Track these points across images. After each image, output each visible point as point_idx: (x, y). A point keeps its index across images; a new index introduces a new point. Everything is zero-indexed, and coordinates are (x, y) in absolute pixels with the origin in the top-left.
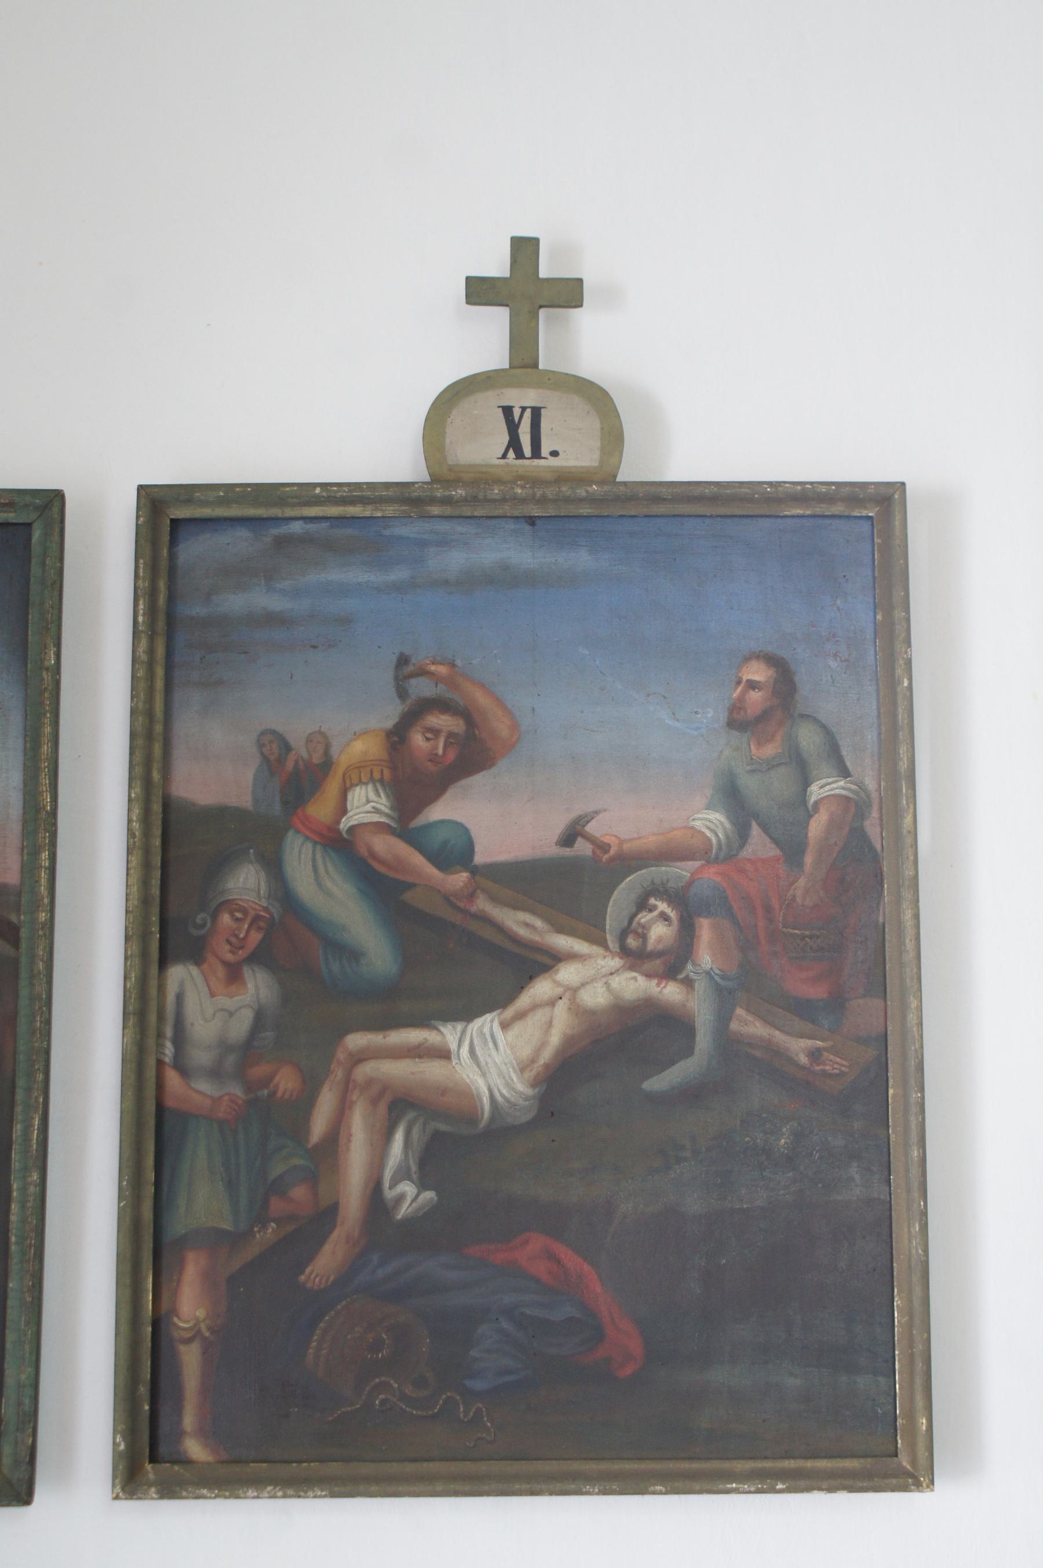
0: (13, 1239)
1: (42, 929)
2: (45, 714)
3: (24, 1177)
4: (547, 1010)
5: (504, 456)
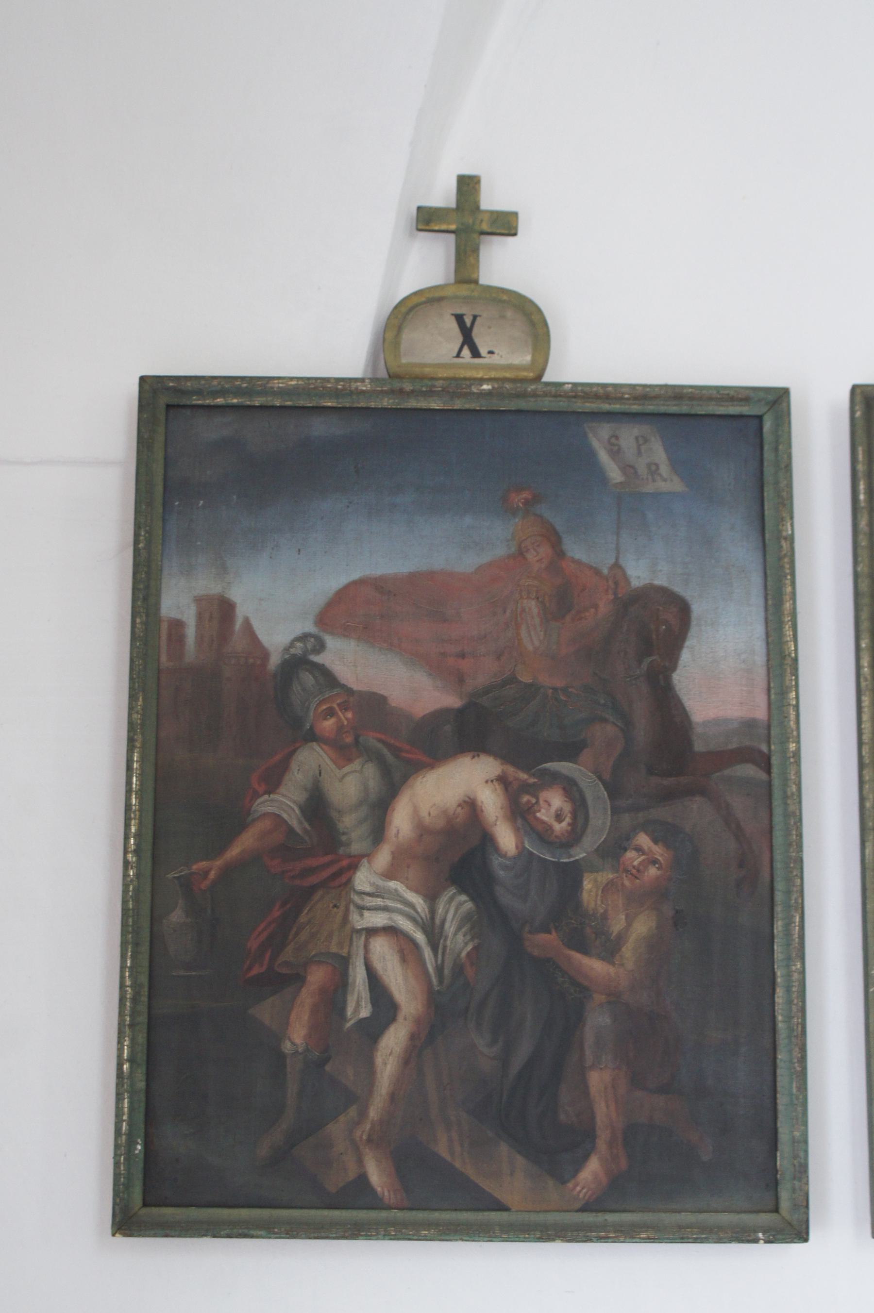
0: (780, 1018)
1: (793, 757)
2: (786, 577)
3: (788, 966)
5: (458, 355)
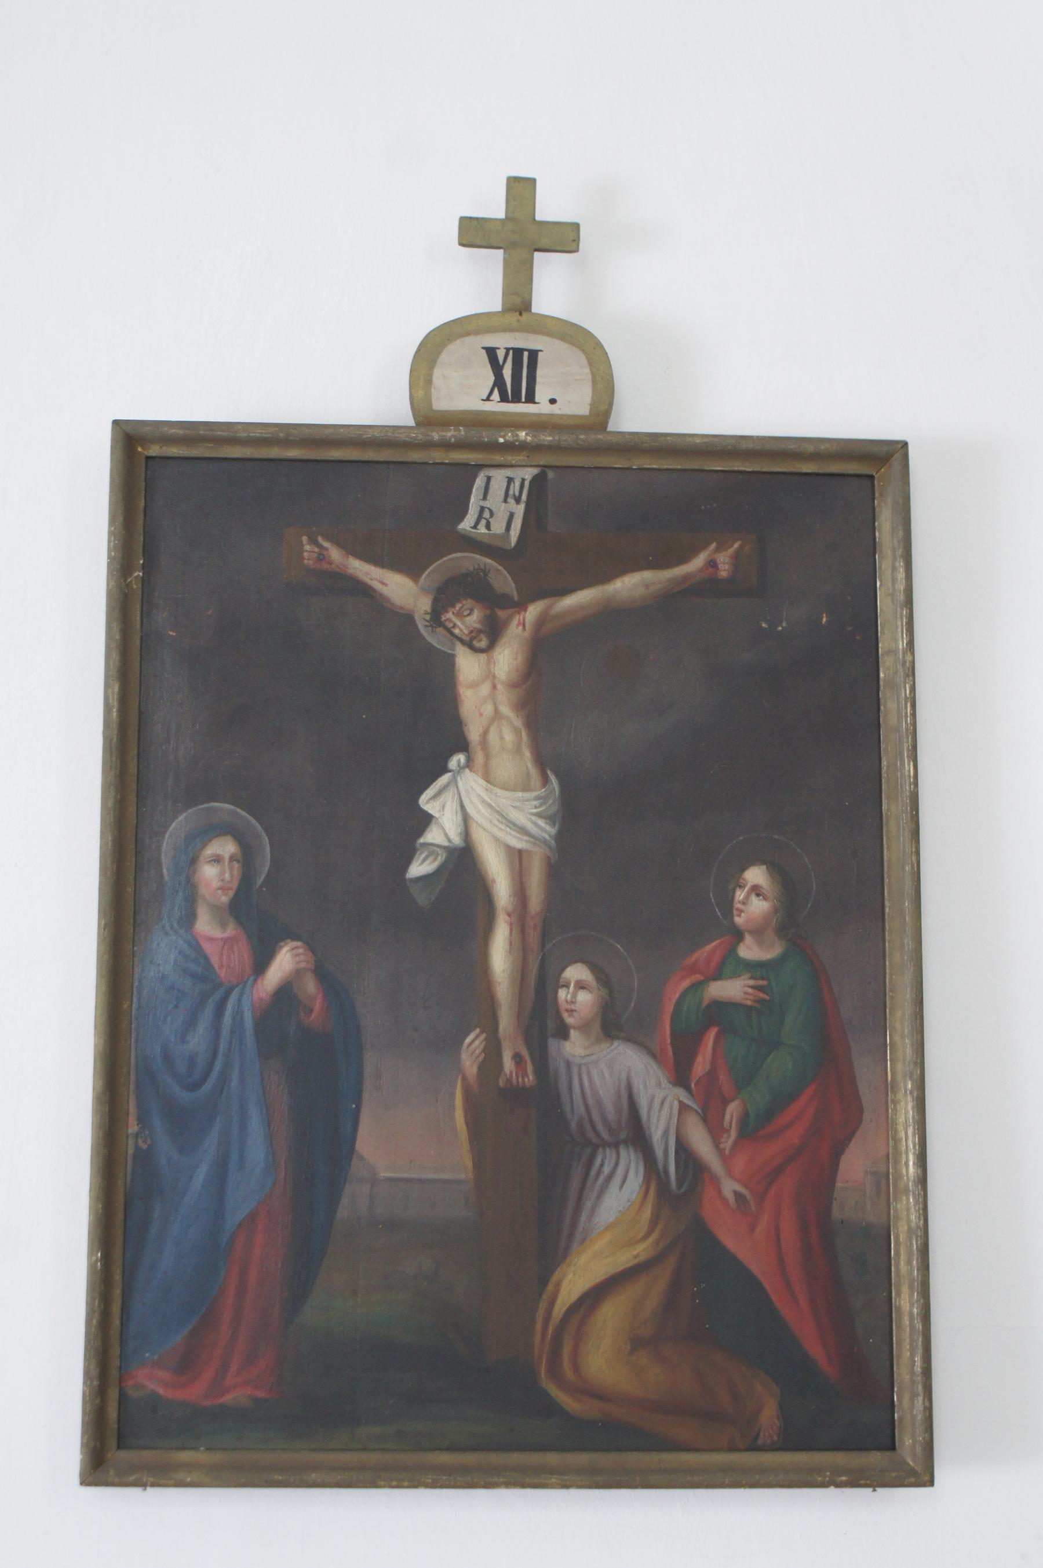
4: (452, 790)
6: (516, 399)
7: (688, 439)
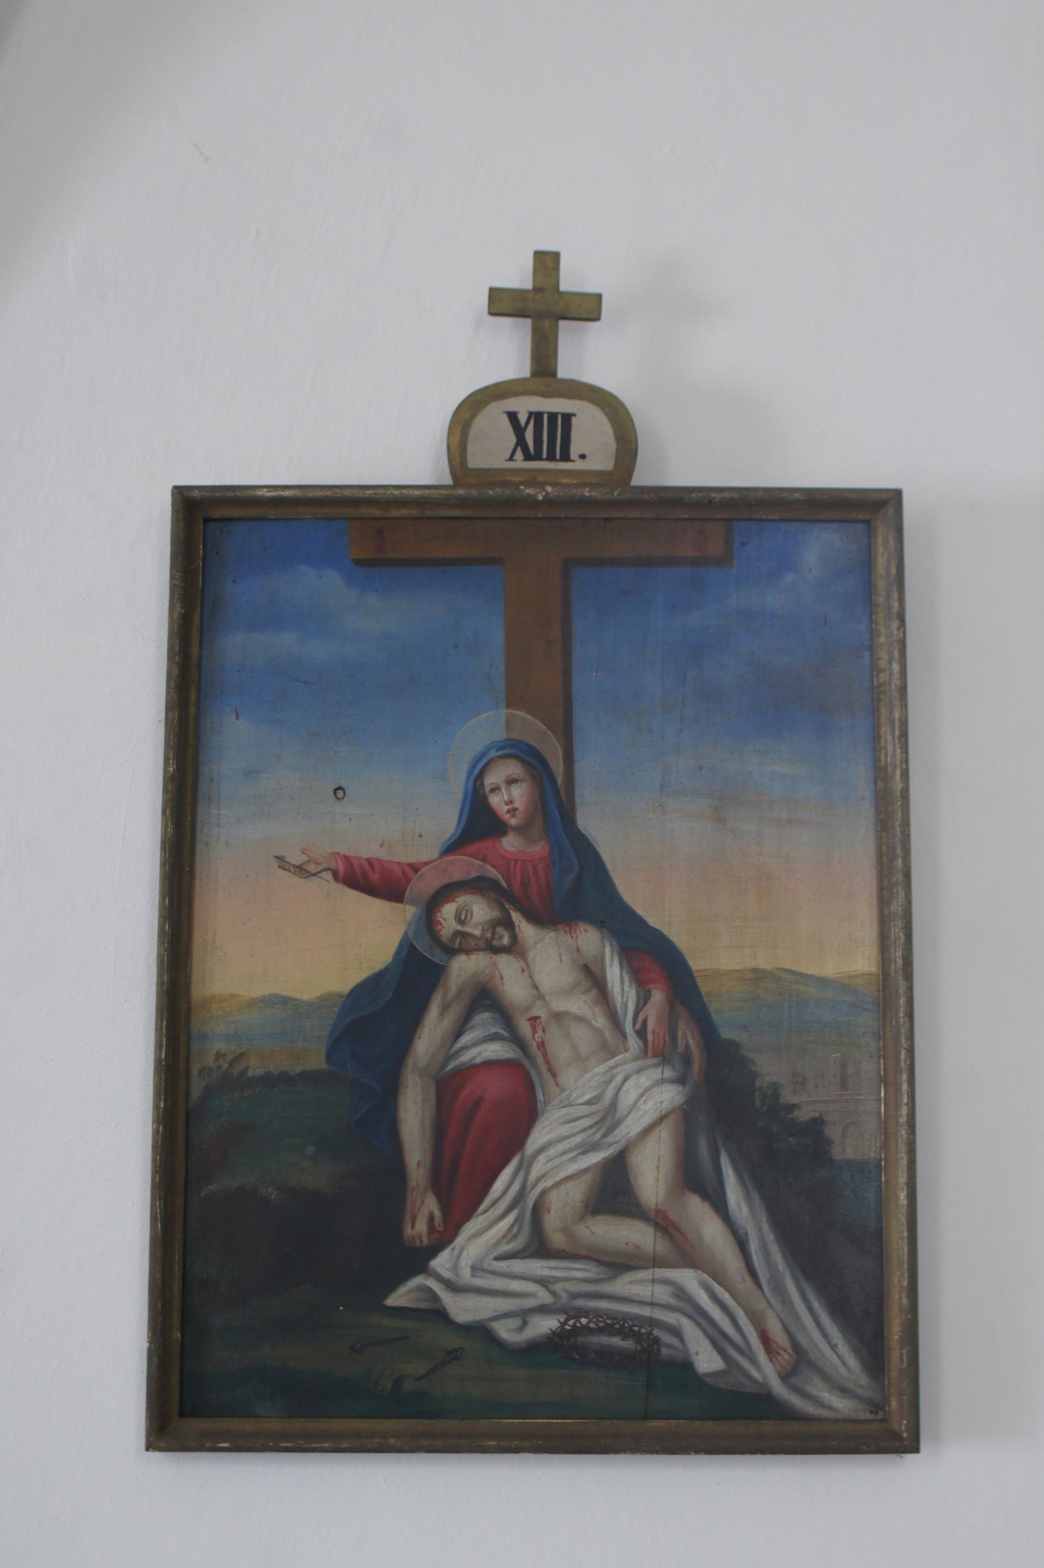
5: (511, 459)
6: (538, 457)
7: (250, 492)
